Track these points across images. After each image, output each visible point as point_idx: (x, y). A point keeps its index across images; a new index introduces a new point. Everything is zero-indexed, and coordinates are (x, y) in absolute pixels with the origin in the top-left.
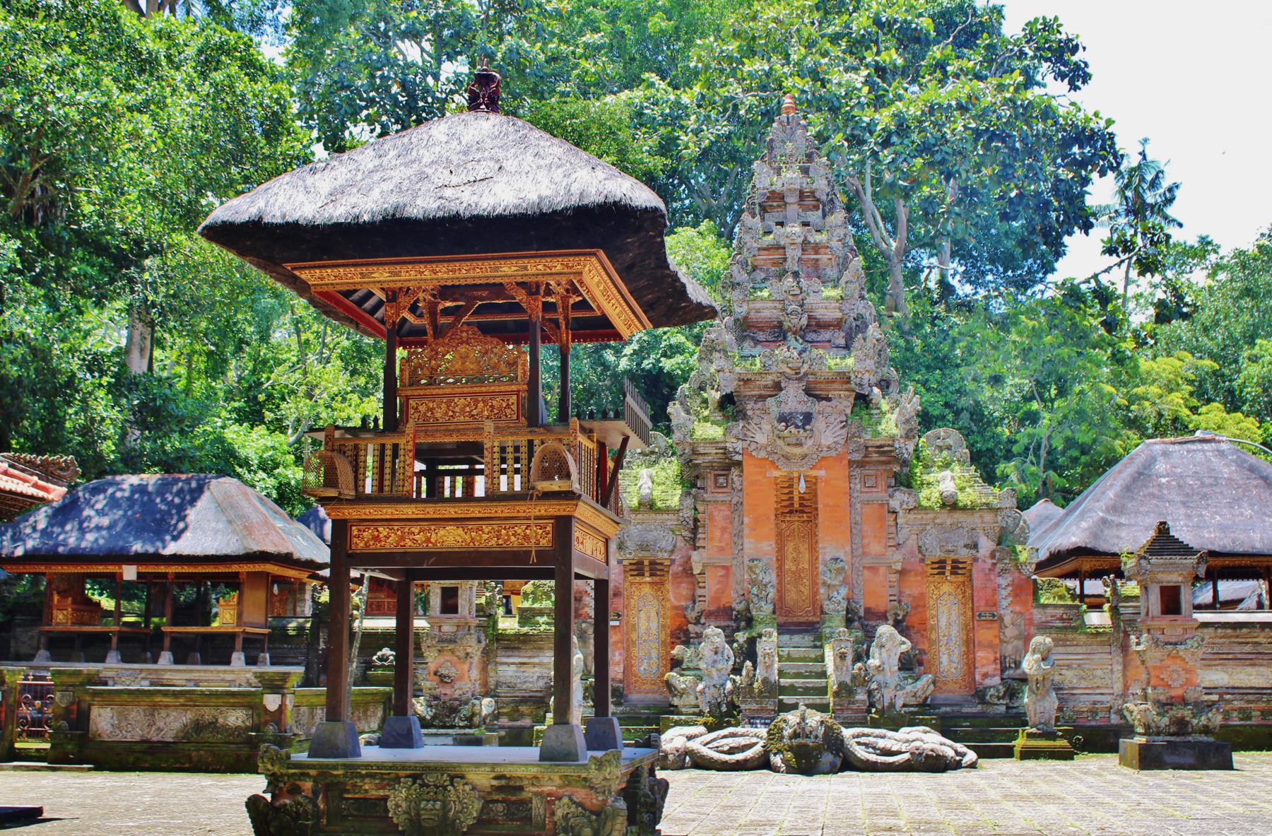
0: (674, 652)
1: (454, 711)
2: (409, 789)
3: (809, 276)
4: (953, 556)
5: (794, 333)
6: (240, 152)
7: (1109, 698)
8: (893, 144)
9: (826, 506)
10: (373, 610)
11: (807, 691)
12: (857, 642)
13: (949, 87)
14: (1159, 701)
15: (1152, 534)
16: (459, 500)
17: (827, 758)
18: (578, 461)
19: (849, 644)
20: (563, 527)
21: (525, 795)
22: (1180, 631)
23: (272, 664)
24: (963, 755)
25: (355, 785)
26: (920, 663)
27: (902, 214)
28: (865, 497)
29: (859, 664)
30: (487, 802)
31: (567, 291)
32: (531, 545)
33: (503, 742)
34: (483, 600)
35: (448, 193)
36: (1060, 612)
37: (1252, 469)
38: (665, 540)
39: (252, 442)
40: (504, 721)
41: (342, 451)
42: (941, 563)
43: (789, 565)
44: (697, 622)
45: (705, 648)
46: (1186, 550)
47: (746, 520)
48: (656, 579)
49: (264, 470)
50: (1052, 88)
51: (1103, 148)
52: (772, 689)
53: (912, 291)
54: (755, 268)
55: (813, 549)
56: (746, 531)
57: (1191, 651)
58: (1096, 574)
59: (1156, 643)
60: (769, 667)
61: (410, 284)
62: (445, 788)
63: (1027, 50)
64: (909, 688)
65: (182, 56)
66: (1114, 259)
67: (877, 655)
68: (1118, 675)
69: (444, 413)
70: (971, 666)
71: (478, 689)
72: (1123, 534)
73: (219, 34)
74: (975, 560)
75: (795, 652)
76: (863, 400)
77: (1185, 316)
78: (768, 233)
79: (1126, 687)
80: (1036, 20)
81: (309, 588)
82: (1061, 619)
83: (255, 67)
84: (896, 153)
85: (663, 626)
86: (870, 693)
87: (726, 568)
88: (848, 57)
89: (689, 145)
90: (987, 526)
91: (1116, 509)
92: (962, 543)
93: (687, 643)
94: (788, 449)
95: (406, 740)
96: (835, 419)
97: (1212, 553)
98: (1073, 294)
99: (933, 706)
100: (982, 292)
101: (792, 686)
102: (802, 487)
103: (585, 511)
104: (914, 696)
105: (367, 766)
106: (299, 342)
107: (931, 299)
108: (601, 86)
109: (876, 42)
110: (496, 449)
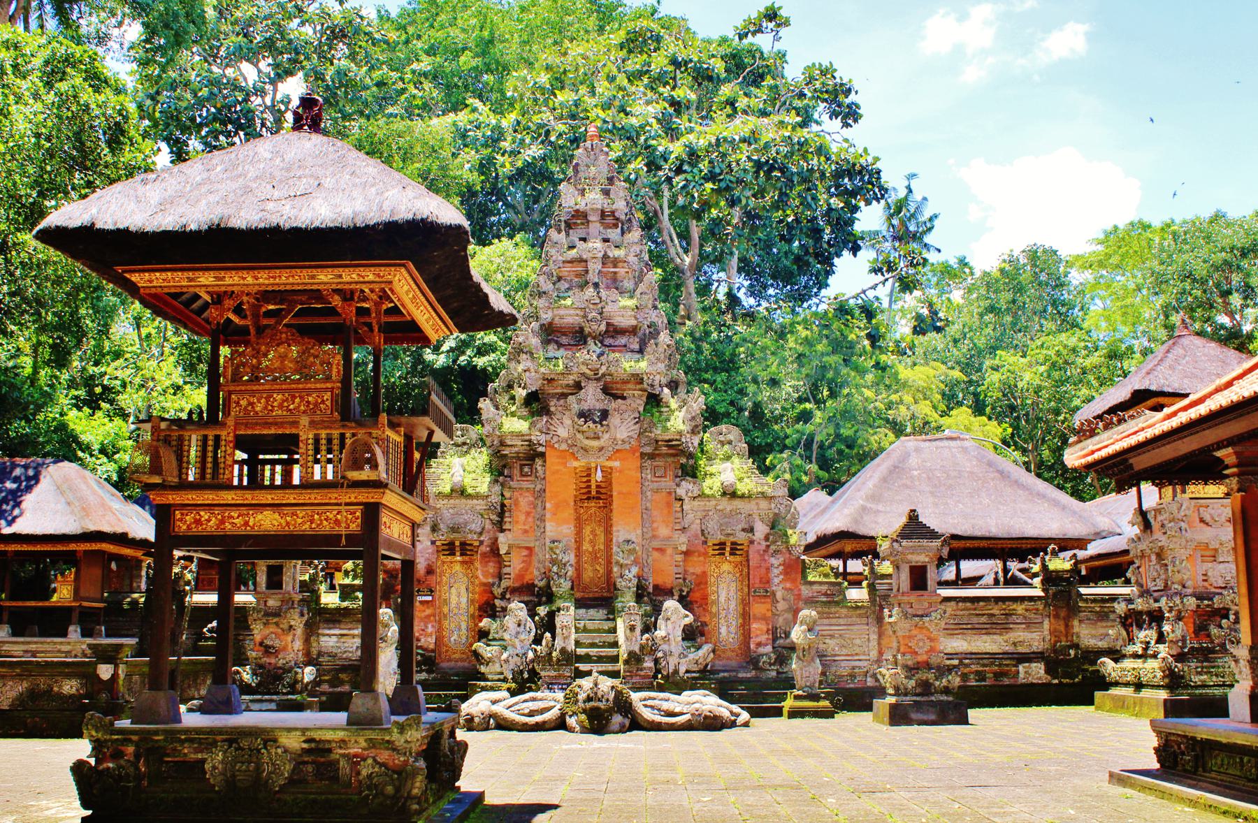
0: (481, 624)
1: (279, 678)
2: (225, 752)
3: (608, 288)
4: (732, 539)
5: (594, 338)
6: (83, 159)
7: (865, 663)
8: (685, 172)
9: (619, 493)
10: (200, 586)
11: (600, 659)
12: (646, 615)
13: (738, 121)
14: (907, 666)
15: (904, 520)
16: (278, 487)
17: (617, 719)
18: (386, 453)
19: (638, 618)
20: (372, 513)
21: (334, 756)
22: (926, 605)
23: (108, 636)
24: (738, 715)
25: (175, 749)
26: (702, 634)
27: (695, 232)
28: (655, 485)
29: (647, 635)
30: (298, 764)
31: (380, 297)
32: (342, 530)
33: (324, 707)
34: (307, 577)
35: (270, 206)
36: (824, 588)
37: (990, 464)
38: (475, 523)
39: (93, 428)
40: (325, 687)
41: (167, 441)
42: (722, 545)
43: (586, 546)
44: (503, 597)
45: (509, 621)
46: (932, 535)
47: (548, 505)
48: (466, 558)
49: (106, 455)
50: (828, 128)
51: (870, 182)
52: (569, 658)
53: (702, 302)
54: (559, 279)
55: (608, 531)
56: (548, 516)
57: (934, 622)
58: (857, 555)
59: (905, 615)
60: (566, 638)
61: (235, 289)
62: (259, 751)
63: (806, 91)
64: (691, 656)
65: (29, 67)
66: (880, 278)
67: (663, 627)
68: (874, 643)
69: (265, 406)
70: (746, 635)
71: (301, 658)
72: (880, 520)
73: (66, 47)
74: (752, 542)
75: (590, 625)
76: (654, 400)
77: (939, 330)
78: (572, 247)
79: (881, 653)
80: (814, 64)
81: (144, 565)
82: (826, 594)
83: (99, 79)
84: (686, 180)
85: (472, 601)
86: (656, 661)
87: (529, 549)
88: (648, 92)
89: (505, 165)
90: (762, 513)
91: (873, 498)
92: (740, 527)
93: (493, 616)
94: (587, 442)
95: (227, 707)
96: (629, 417)
97: (954, 537)
98: (843, 310)
99: (713, 672)
100: (764, 304)
101: (587, 655)
102: (599, 476)
103: (392, 499)
104: (696, 663)
105: (188, 731)
106: (139, 336)
107: (719, 309)
108: (427, 108)
109: (674, 79)
110: (310, 441)
